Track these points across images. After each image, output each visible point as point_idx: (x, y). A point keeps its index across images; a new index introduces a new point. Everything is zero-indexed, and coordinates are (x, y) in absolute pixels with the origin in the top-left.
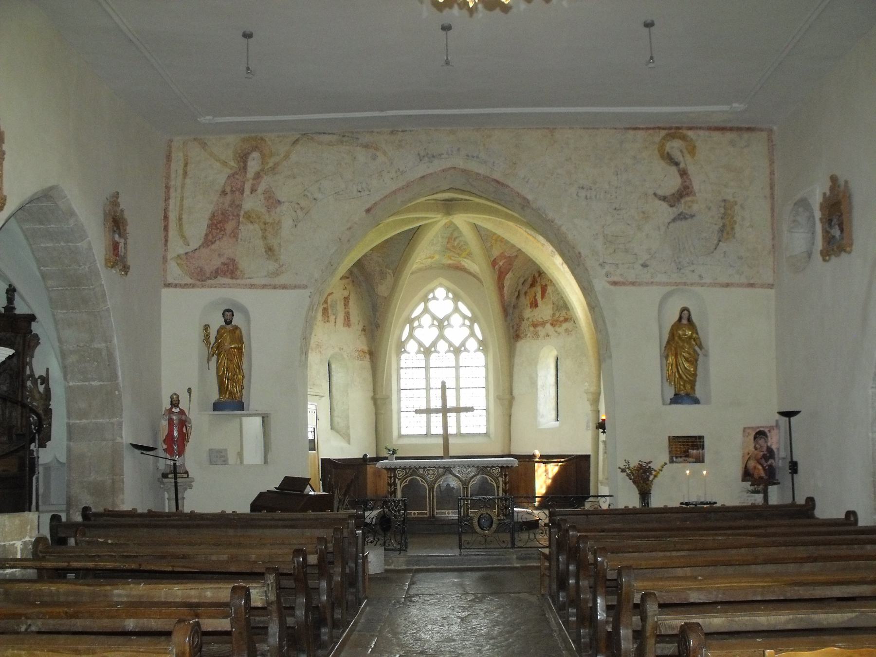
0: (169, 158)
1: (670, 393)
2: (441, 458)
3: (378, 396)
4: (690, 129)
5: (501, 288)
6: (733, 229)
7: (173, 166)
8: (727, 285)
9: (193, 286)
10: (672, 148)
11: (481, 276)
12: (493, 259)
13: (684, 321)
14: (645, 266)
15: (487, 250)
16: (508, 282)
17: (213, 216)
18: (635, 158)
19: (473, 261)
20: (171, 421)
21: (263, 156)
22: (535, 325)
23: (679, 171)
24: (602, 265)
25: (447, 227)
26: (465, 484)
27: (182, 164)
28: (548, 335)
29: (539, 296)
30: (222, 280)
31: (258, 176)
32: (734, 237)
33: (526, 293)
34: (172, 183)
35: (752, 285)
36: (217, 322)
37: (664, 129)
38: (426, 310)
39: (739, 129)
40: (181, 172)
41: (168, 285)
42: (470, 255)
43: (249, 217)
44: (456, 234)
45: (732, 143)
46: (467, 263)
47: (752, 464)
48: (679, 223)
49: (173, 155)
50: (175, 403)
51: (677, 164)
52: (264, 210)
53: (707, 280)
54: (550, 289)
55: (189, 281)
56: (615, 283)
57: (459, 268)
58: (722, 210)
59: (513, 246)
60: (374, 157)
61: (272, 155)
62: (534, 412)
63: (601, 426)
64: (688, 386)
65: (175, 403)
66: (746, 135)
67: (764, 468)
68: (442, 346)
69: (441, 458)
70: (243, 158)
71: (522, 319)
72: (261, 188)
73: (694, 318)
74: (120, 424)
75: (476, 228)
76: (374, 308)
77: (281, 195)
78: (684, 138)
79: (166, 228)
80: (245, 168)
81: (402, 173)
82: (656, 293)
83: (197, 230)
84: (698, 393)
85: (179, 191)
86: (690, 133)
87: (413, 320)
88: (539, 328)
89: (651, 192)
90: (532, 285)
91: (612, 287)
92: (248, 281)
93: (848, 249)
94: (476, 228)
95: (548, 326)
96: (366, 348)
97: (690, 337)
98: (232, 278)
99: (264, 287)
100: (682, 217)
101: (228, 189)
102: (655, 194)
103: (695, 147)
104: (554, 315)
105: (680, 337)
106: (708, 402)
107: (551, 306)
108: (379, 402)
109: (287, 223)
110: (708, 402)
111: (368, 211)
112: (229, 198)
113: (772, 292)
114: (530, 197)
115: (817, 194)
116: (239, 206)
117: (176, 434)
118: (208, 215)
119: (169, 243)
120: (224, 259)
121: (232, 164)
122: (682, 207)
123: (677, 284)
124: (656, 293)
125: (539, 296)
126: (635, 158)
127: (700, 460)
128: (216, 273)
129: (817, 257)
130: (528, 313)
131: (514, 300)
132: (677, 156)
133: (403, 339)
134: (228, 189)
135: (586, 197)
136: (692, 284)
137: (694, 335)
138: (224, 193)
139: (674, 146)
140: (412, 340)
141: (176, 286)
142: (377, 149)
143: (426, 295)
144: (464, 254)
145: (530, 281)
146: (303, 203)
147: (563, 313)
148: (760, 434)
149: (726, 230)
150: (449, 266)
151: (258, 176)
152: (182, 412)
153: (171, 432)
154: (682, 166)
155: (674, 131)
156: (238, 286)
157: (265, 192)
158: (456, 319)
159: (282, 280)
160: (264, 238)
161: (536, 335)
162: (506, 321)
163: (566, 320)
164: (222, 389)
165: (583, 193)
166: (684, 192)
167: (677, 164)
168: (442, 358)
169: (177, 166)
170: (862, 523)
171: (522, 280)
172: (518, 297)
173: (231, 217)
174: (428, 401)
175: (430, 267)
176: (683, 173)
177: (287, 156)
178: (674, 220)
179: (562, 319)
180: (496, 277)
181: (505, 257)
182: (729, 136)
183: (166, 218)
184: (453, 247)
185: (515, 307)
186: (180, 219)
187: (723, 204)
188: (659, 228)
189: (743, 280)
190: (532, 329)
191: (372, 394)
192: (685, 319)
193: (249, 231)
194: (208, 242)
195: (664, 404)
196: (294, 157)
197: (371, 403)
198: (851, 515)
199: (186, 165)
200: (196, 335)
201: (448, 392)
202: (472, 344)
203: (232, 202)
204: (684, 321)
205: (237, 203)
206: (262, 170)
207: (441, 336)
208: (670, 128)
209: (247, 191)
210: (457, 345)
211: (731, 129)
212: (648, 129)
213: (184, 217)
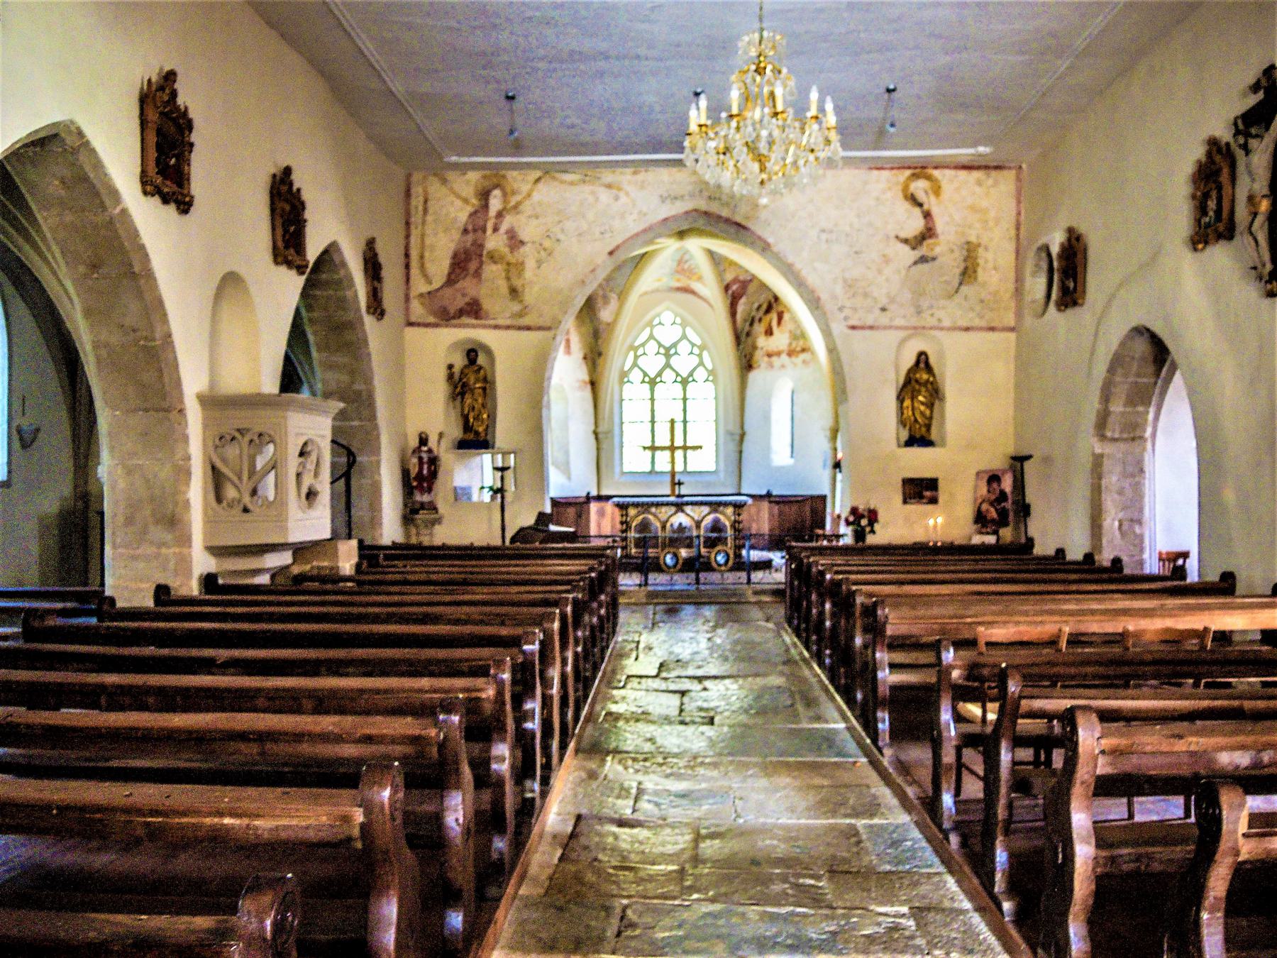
0: (408, 194)
1: (905, 435)
2: (668, 496)
3: (600, 430)
4: (936, 168)
5: (733, 313)
6: (975, 272)
7: (414, 202)
8: (967, 329)
9: (436, 325)
10: (916, 188)
11: (713, 302)
12: (725, 283)
13: (922, 365)
14: (883, 309)
15: (720, 274)
16: (741, 307)
17: (455, 256)
18: (878, 199)
19: (704, 284)
20: (420, 459)
21: (505, 195)
22: (769, 355)
23: (923, 212)
24: (841, 309)
25: (678, 250)
26: (698, 524)
27: (421, 199)
28: (783, 366)
29: (774, 323)
30: (465, 320)
31: (500, 215)
32: (976, 279)
33: (760, 320)
34: (413, 219)
35: (992, 329)
36: (459, 361)
37: (909, 168)
38: (651, 337)
39: (987, 167)
40: (421, 208)
41: (411, 324)
42: (700, 279)
43: (493, 258)
44: (686, 257)
45: (979, 183)
46: (696, 286)
47: (985, 507)
48: (920, 266)
49: (413, 191)
50: (423, 440)
51: (920, 205)
52: (507, 250)
53: (946, 323)
54: (786, 317)
55: (431, 319)
56: (853, 328)
57: (687, 290)
58: (965, 253)
59: (747, 271)
60: (617, 198)
61: (514, 193)
62: (767, 449)
63: (837, 465)
64: (924, 429)
65: (423, 440)
66: (994, 173)
67: (996, 510)
68: (668, 375)
69: (668, 496)
70: (485, 195)
71: (755, 347)
72: (504, 227)
73: (932, 361)
74: (378, 462)
75: (711, 254)
76: (596, 335)
77: (524, 235)
78: (929, 178)
79: (407, 266)
80: (486, 206)
81: (645, 215)
82: (894, 337)
83: (439, 267)
84: (934, 435)
85: (420, 227)
86: (936, 173)
87: (636, 349)
88: (774, 359)
89: (892, 235)
90: (768, 310)
91: (850, 332)
92: (492, 322)
93: (1080, 301)
94: (711, 254)
95: (784, 357)
96: (587, 378)
97: (928, 381)
98: (476, 318)
99: (508, 327)
100: (923, 259)
101: (470, 227)
102: (897, 237)
103: (939, 187)
104: (790, 344)
105: (917, 381)
106: (943, 445)
107: (787, 335)
108: (600, 436)
109: (530, 264)
110: (943, 445)
111: (611, 253)
112: (470, 237)
113: (1012, 336)
114: (770, 240)
115: (1056, 241)
116: (481, 246)
117: (425, 472)
118: (450, 254)
119: (411, 282)
120: (467, 300)
121: (474, 201)
122: (923, 250)
123: (915, 328)
124: (894, 337)
125: (774, 323)
126: (878, 199)
127: (934, 501)
128: (461, 313)
129: (1052, 307)
130: (762, 342)
131: (747, 328)
132: (921, 197)
133: (626, 368)
134: (470, 227)
135: (827, 241)
136: (931, 328)
137: (931, 379)
138: (465, 231)
139: (919, 187)
140: (636, 369)
141: (419, 325)
142: (620, 189)
143: (651, 321)
144: (694, 278)
145: (765, 307)
146: (547, 243)
147: (801, 343)
148: (994, 479)
149: (968, 272)
150: (679, 289)
151: (500, 215)
152: (430, 451)
153: (421, 469)
154: (926, 207)
155: (920, 170)
156: (485, 327)
157: (507, 232)
158: (684, 347)
159: (526, 321)
160: (508, 279)
161: (771, 366)
162: (738, 350)
163: (803, 350)
164: (467, 427)
165: (824, 236)
166: (928, 233)
167: (920, 205)
168: (668, 391)
169: (417, 202)
170: (1127, 571)
171: (756, 305)
172: (752, 324)
173: (474, 257)
174: (672, 440)
175: (657, 291)
176: (927, 215)
177: (529, 195)
178: (915, 263)
179: (799, 349)
180: (729, 302)
181: (739, 281)
182: (976, 174)
183: (407, 255)
184: (683, 270)
185: (748, 334)
186: (422, 257)
187: (966, 247)
188: (899, 272)
189: (983, 324)
190: (766, 359)
191: (593, 428)
192: (922, 361)
193: (492, 271)
194: (451, 281)
195: (899, 446)
196: (536, 196)
197: (593, 437)
198: (1060, 552)
199: (426, 201)
200: (442, 374)
201: (676, 425)
202: (701, 374)
203: (474, 243)
204: (922, 365)
205: (479, 242)
206: (504, 209)
207: (668, 365)
208: (916, 168)
209: (489, 231)
210: (685, 375)
211: (978, 168)
212: (892, 169)
213: (427, 254)
